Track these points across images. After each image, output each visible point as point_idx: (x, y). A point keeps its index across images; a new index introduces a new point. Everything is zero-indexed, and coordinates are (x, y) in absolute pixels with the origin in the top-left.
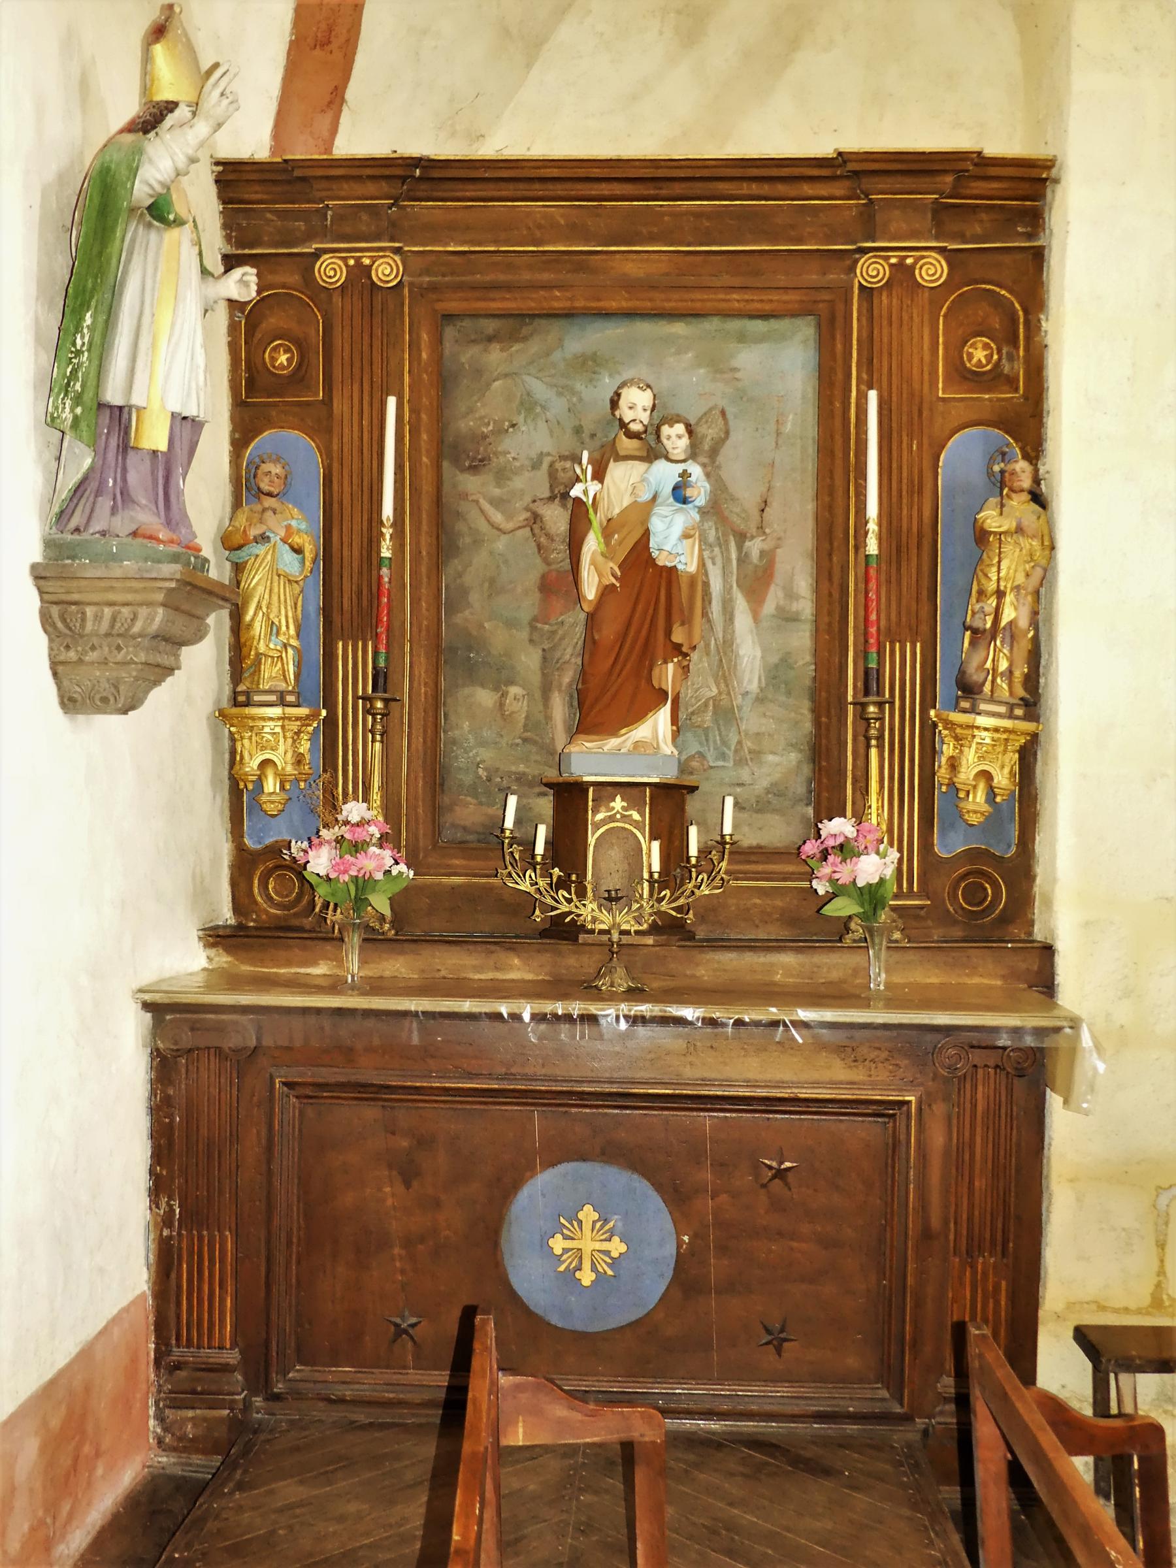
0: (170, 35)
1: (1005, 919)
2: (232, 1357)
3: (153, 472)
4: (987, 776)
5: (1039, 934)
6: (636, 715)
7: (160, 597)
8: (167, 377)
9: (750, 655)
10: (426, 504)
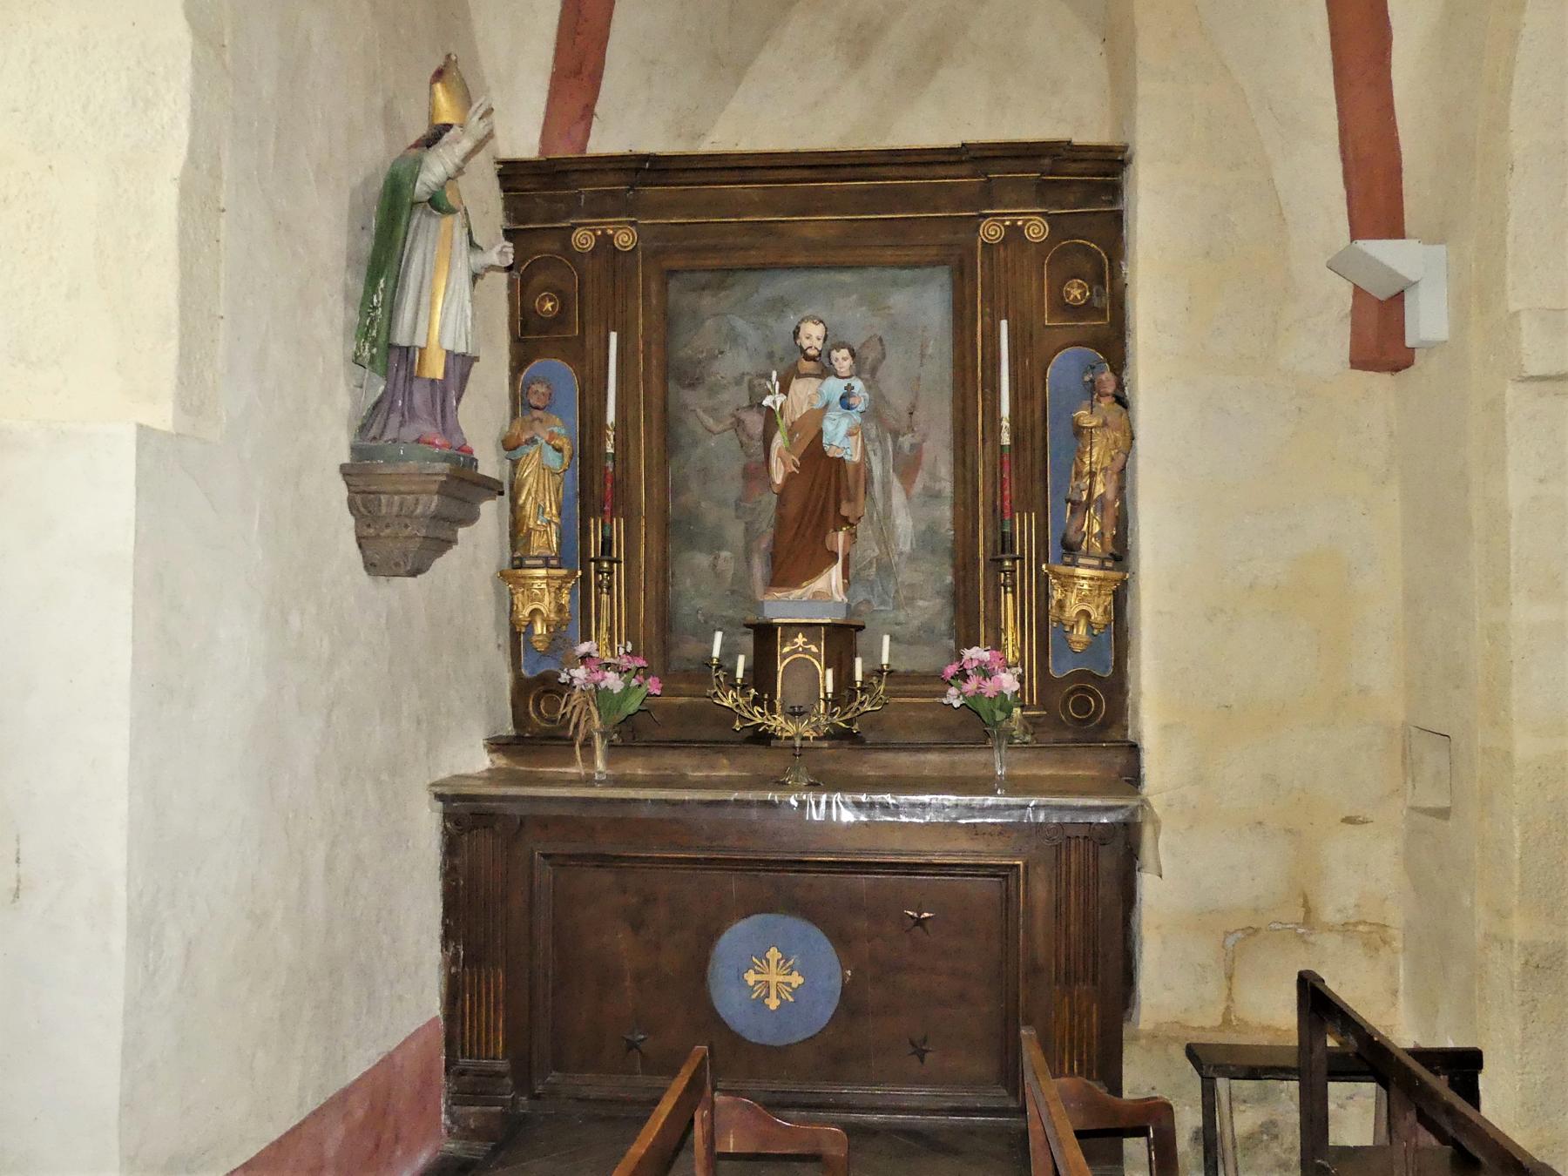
0: (447, 77)
1: (1106, 725)
2: (502, 1065)
3: (433, 396)
4: (1087, 614)
5: (1130, 736)
6: (815, 572)
7: (435, 487)
8: (442, 327)
9: (904, 524)
10: (655, 415)
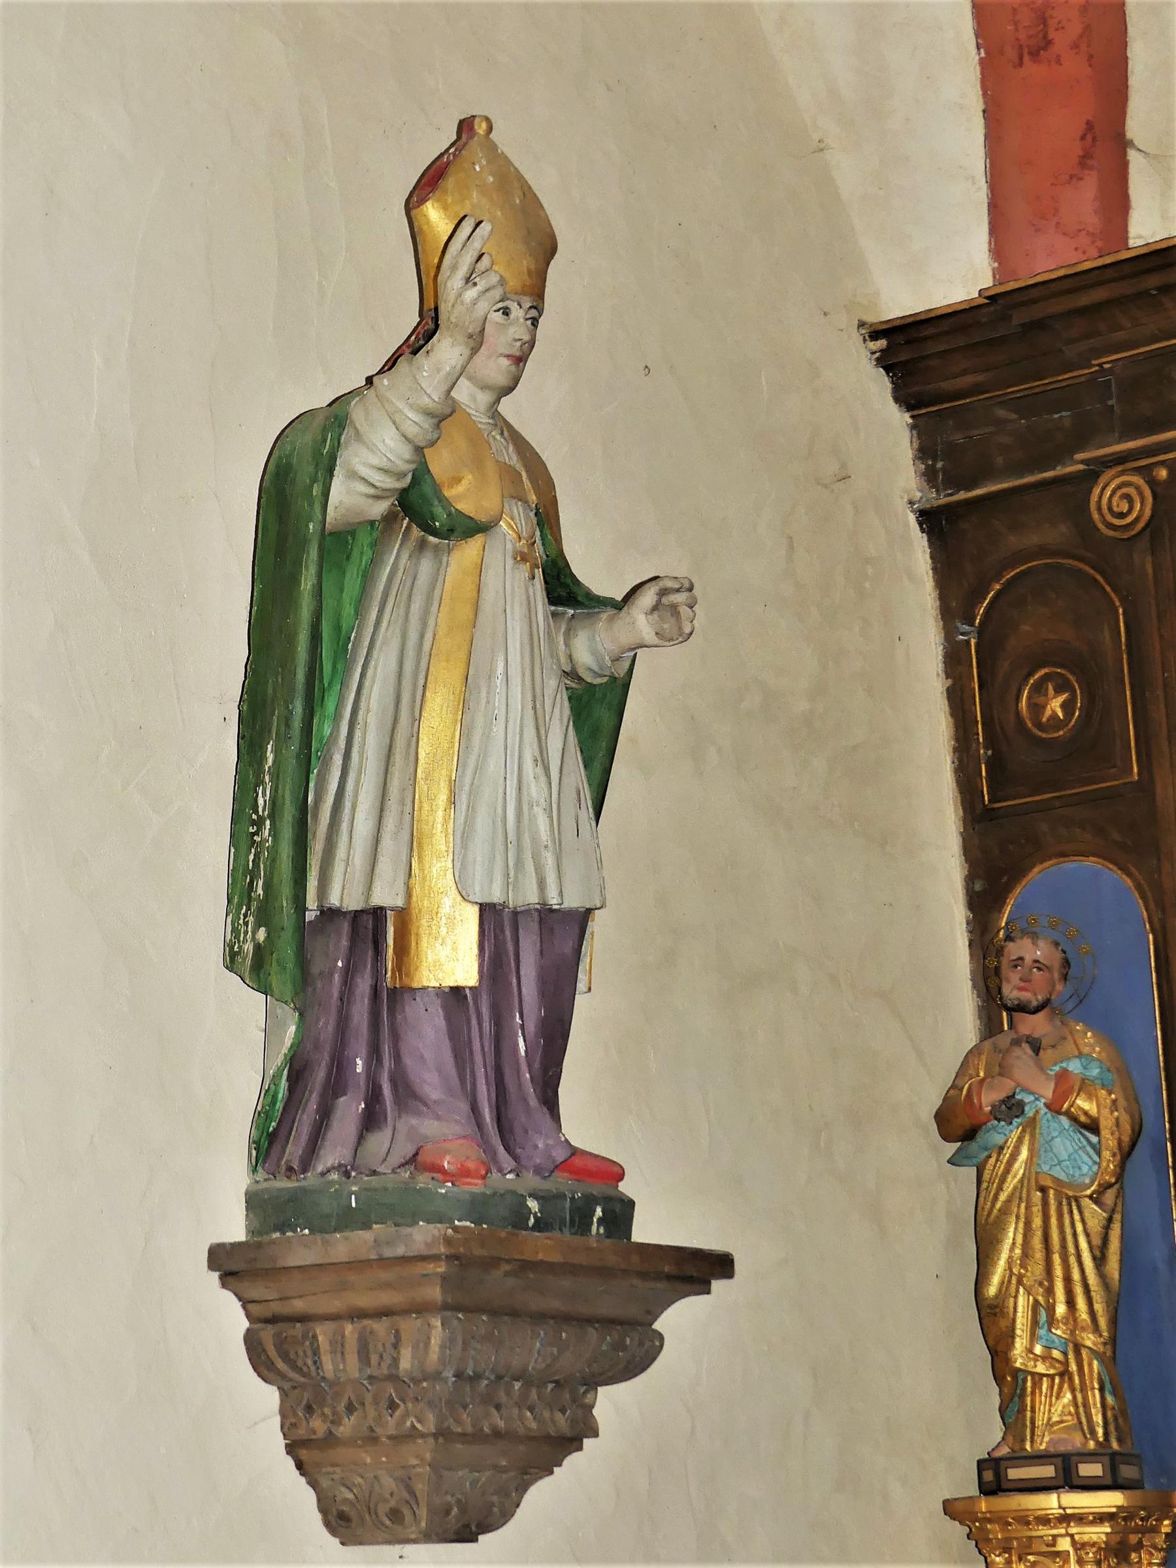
0: (450, 182)
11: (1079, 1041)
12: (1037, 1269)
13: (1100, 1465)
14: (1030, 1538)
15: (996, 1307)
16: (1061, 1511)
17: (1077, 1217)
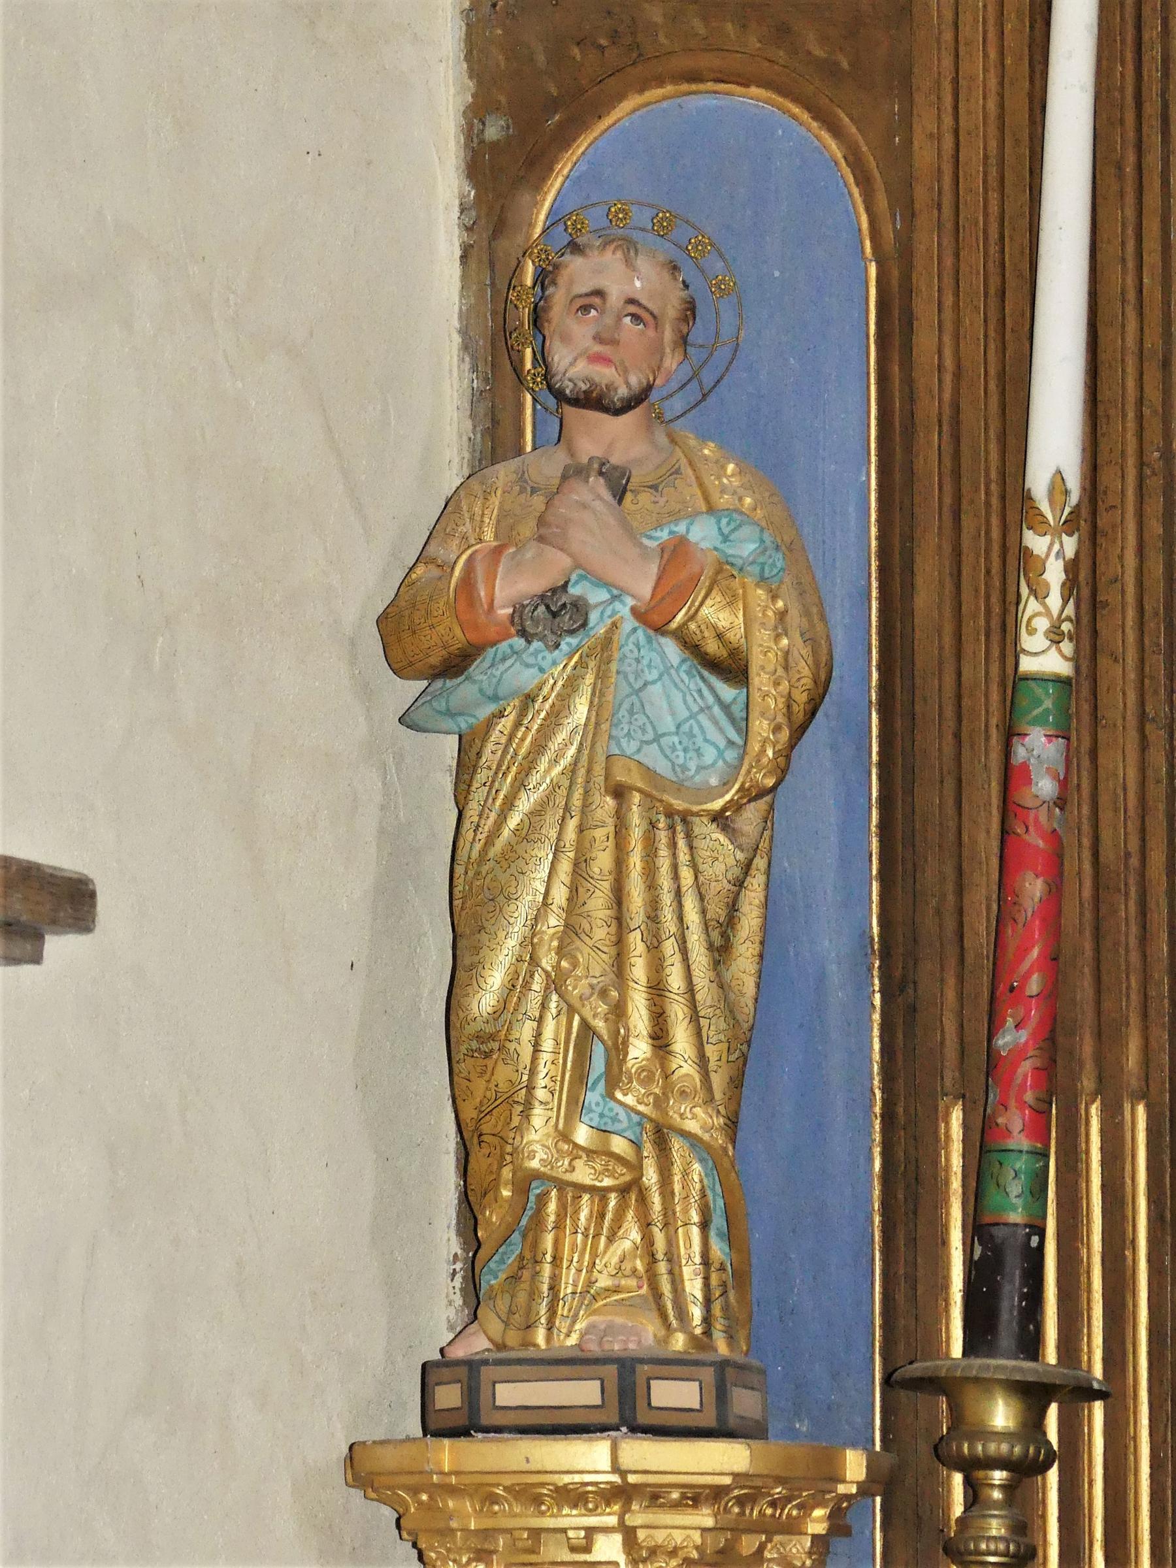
11: (711, 481)
12: (593, 962)
13: (695, 1385)
14: (536, 1533)
15: (492, 1037)
16: (615, 1478)
17: (683, 856)
